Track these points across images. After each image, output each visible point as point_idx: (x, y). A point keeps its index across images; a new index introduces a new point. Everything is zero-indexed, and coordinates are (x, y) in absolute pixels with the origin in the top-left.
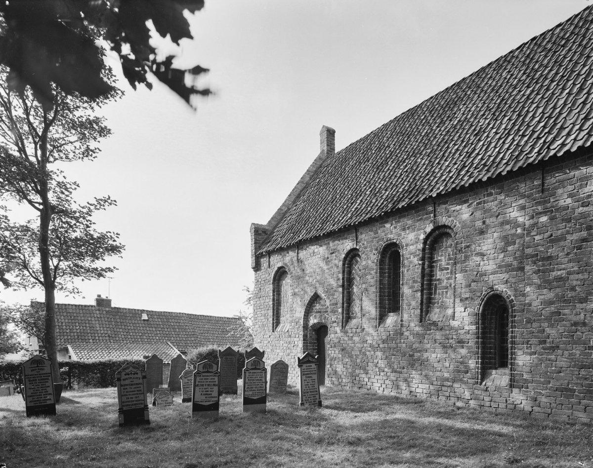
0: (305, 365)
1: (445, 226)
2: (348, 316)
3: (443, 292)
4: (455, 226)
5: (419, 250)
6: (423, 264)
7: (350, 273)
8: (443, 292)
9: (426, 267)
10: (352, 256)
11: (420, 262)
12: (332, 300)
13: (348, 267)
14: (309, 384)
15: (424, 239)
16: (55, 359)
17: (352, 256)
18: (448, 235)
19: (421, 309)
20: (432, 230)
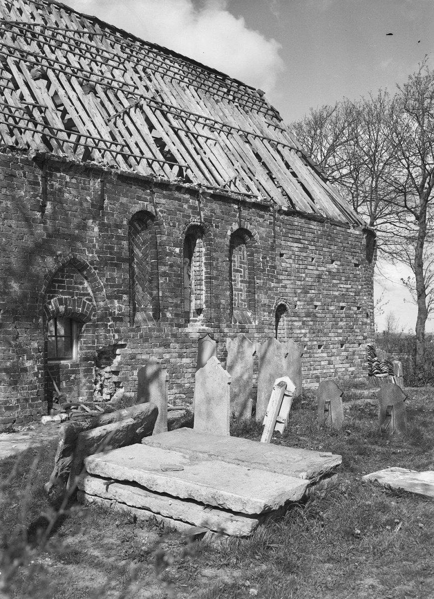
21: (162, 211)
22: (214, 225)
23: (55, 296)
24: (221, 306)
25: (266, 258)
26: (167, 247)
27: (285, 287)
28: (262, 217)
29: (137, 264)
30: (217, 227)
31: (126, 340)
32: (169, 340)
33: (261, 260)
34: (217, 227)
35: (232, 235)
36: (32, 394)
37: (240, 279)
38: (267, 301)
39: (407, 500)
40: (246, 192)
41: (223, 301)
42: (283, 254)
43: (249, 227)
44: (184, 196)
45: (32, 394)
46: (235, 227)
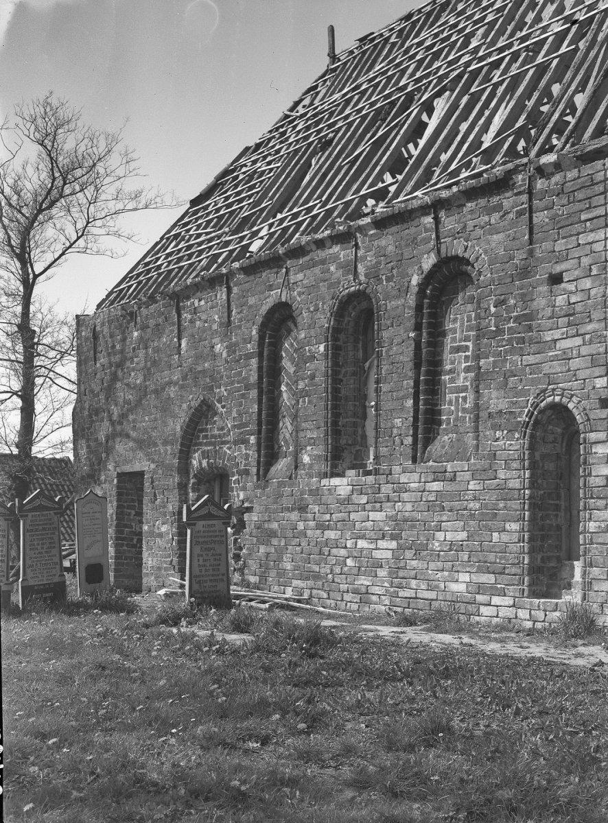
0: (202, 523)
1: (456, 258)
2: (269, 453)
3: (457, 399)
4: (477, 258)
5: (409, 308)
6: (419, 336)
7: (275, 358)
8: (457, 399)
9: (423, 346)
10: (280, 320)
11: (412, 335)
12: (235, 414)
13: (270, 344)
14: (208, 564)
15: (419, 285)
16: (383, 174)
17: (280, 320)
18: (466, 279)
19: (415, 436)
20: (434, 266)
21: (300, 294)
22: (384, 277)
23: (198, 449)
24: (395, 431)
25: (503, 302)
26: (307, 348)
27: (566, 357)
28: (498, 208)
29: (287, 385)
30: (389, 279)
31: (251, 502)
32: (306, 499)
33: (493, 310)
34: (389, 279)
35: (422, 287)
36: (165, 562)
37: (464, 365)
38: (503, 405)
39: (48, 729)
40: (264, 241)
41: (398, 422)
42: (561, 274)
43: (457, 248)
44: (331, 251)
45: (165, 562)
46: (429, 261)
